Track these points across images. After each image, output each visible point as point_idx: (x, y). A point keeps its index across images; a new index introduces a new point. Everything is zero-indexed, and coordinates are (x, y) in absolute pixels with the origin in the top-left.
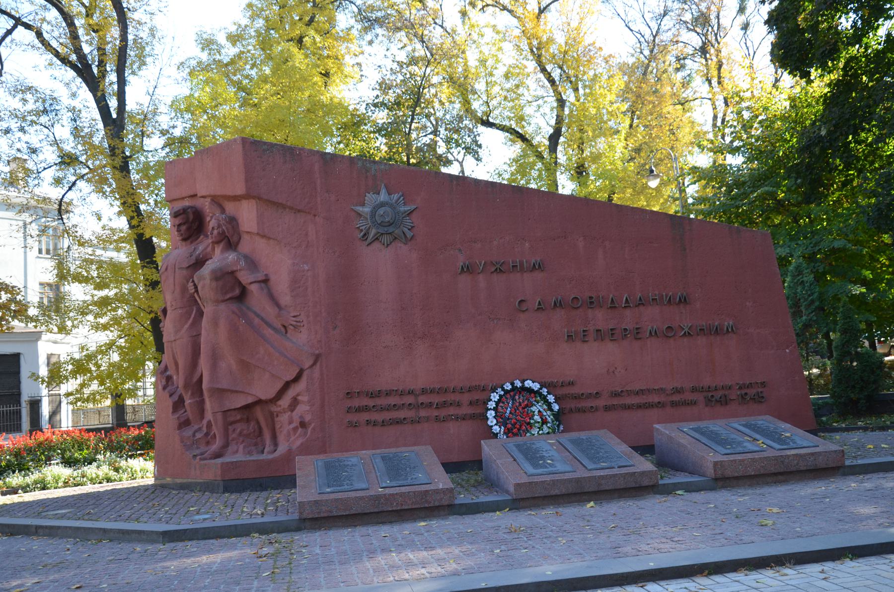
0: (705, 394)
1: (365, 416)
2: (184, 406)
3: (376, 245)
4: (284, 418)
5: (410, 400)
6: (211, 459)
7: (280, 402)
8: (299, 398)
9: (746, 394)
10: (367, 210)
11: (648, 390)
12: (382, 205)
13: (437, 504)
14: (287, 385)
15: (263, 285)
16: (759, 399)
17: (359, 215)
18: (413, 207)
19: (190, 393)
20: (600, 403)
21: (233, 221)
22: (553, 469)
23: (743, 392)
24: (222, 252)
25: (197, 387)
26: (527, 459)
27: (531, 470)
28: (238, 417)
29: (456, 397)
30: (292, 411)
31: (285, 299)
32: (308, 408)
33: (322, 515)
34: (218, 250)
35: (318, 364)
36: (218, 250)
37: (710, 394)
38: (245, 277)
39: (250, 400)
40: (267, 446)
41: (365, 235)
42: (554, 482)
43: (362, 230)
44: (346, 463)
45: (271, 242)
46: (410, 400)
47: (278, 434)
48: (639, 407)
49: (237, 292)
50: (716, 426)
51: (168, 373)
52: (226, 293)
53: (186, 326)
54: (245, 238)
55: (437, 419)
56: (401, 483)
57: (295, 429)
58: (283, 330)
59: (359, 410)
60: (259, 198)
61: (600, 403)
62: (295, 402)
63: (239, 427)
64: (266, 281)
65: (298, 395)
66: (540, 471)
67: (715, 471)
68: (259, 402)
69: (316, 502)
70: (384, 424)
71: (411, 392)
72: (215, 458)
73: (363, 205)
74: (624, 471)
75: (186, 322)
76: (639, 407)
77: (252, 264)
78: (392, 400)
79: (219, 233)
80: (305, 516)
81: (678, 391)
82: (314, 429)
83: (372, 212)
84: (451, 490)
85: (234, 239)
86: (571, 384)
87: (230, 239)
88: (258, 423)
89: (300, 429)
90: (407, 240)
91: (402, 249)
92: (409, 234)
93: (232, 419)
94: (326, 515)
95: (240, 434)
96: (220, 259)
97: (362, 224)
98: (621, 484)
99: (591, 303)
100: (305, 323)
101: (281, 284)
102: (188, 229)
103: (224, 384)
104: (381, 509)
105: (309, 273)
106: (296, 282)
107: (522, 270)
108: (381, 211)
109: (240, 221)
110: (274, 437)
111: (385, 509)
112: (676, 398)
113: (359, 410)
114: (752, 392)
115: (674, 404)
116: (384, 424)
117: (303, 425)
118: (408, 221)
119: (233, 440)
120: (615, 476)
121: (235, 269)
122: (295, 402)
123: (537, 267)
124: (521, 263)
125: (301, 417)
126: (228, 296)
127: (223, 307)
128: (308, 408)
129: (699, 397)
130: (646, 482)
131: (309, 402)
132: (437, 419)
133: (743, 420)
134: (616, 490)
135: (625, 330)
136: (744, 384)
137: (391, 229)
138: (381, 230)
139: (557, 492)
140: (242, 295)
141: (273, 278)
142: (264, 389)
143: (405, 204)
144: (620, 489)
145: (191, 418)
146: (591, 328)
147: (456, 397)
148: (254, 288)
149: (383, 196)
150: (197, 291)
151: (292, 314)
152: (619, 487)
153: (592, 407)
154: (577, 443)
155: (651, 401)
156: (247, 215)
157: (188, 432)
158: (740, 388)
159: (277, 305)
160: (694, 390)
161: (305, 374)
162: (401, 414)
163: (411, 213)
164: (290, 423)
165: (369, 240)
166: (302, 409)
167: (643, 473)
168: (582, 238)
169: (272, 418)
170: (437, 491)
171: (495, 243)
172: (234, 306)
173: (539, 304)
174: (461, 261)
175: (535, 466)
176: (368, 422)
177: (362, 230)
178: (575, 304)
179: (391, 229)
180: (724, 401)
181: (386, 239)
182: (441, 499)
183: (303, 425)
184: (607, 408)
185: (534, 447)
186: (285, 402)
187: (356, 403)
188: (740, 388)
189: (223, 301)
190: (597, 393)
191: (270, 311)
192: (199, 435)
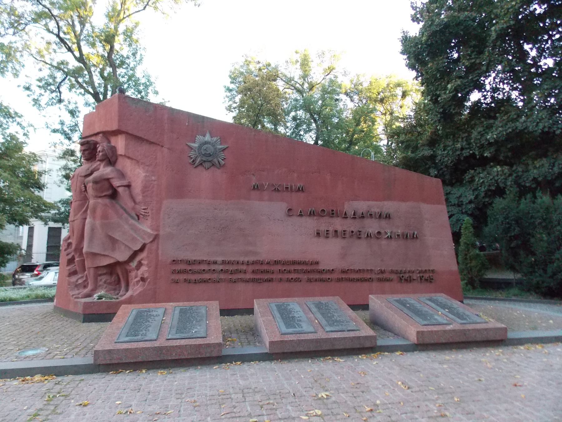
0: (399, 275)
1: (185, 276)
2: (74, 262)
3: (200, 168)
4: (133, 274)
6: (82, 298)
7: (131, 264)
8: (143, 262)
9: (423, 276)
10: (196, 145)
11: (364, 270)
12: (206, 143)
13: (208, 355)
15: (126, 188)
16: (430, 280)
17: (191, 148)
18: (226, 146)
19: (78, 254)
20: (334, 276)
21: (113, 149)
22: (300, 329)
23: (421, 275)
24: (104, 167)
25: (79, 249)
26: (283, 318)
27: (284, 329)
28: (105, 272)
29: (244, 267)
31: (139, 198)
32: (147, 269)
33: (113, 362)
34: (102, 166)
35: (156, 241)
36: (102, 166)
37: (401, 275)
38: (116, 183)
39: (112, 261)
40: (121, 291)
41: (193, 161)
42: (300, 342)
43: (192, 158)
44: (151, 313)
45: (134, 161)
47: (130, 281)
48: (358, 280)
49: (110, 192)
50: (411, 299)
51: (69, 241)
52: (102, 192)
53: (80, 213)
54: (120, 160)
55: (231, 281)
56: (183, 335)
57: (138, 282)
58: (136, 218)
59: (180, 272)
60: (126, 133)
61: (334, 276)
63: (104, 278)
64: (129, 186)
65: (142, 260)
66: (290, 330)
67: (418, 338)
69: (109, 351)
70: (195, 282)
72: (85, 297)
73: (194, 142)
74: (352, 334)
75: (81, 211)
76: (358, 280)
77: (122, 175)
78: (203, 267)
79: (102, 155)
80: (99, 362)
81: (382, 272)
82: (149, 283)
83: (199, 146)
84: (219, 345)
85: (113, 160)
87: (111, 159)
88: (118, 275)
89: (141, 282)
90: (221, 166)
91: (218, 172)
92: (223, 162)
93: (100, 272)
94: (116, 362)
95: (105, 282)
96: (105, 171)
97: (192, 154)
98: (349, 345)
99: (333, 214)
100: (150, 214)
101: (137, 188)
102: (89, 153)
103: (96, 250)
104: (162, 358)
105: (155, 183)
106: (145, 189)
107: (292, 191)
108: (205, 147)
109: (117, 148)
110: (127, 285)
111: (166, 358)
112: (380, 276)
113: (180, 272)
114: (426, 276)
115: (380, 280)
116: (195, 282)
117: (143, 279)
118: (222, 155)
119: (100, 286)
120: (345, 338)
121: (110, 177)
122: (140, 264)
123: (300, 190)
124: (291, 187)
125: (143, 274)
126: (104, 194)
127: (100, 200)
128: (147, 269)
129: (393, 276)
130: (368, 345)
131: (148, 264)
132: (231, 281)
133: (428, 296)
134: (345, 349)
135: (352, 232)
136: (422, 270)
137: (210, 159)
138: (204, 159)
139: (302, 349)
140: (114, 195)
141: (133, 184)
142: (121, 256)
143: (221, 144)
144: (348, 349)
145: (78, 270)
146: (331, 229)
147: (244, 267)
148: (120, 190)
149: (208, 138)
151: (143, 208)
152: (348, 347)
153: (329, 279)
154: (319, 306)
155: (365, 276)
156: (120, 143)
157: (74, 279)
158: (419, 273)
159: (134, 202)
160: (392, 272)
161: (147, 246)
162: (206, 276)
164: (136, 277)
165: (196, 164)
166: (144, 268)
167: (366, 338)
168: (329, 174)
169: (127, 273)
170: (209, 345)
171: (276, 172)
172: (107, 201)
173: (301, 212)
174: (254, 181)
175: (288, 325)
176: (185, 280)
177: (192, 158)
178: (321, 214)
179: (210, 159)
180: (409, 280)
181: (207, 165)
182: (212, 351)
183: (143, 279)
184: (339, 280)
185: (289, 307)
186: (134, 264)
188: (419, 273)
189: (100, 197)
190: (333, 270)
191: (130, 204)
192: (80, 281)
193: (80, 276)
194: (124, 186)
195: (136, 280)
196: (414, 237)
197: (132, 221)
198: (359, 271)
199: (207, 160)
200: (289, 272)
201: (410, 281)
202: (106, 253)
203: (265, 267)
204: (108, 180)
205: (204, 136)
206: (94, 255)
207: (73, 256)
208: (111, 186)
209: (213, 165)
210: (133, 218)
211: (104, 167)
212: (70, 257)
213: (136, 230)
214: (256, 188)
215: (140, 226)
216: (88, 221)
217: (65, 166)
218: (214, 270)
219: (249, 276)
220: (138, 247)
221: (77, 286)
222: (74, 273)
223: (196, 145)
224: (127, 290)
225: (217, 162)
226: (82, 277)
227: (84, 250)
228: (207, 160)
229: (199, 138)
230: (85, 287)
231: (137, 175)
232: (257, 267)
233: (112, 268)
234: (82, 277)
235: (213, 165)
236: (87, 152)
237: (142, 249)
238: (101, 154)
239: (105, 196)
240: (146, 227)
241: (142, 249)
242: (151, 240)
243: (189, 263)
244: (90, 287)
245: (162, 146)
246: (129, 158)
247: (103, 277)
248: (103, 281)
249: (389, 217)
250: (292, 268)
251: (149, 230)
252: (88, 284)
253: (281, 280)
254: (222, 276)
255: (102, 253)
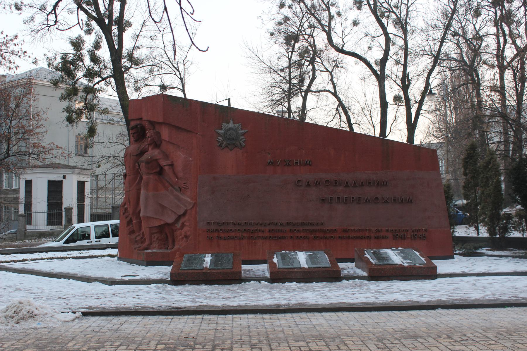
5: (237, 228)
7: (176, 225)
8: (185, 223)
12: (230, 129)
14: (180, 217)
17: (219, 134)
24: (152, 149)
29: (262, 228)
30: (182, 229)
31: (181, 175)
32: (189, 229)
34: (150, 148)
38: (163, 163)
39: (162, 223)
41: (221, 144)
46: (237, 228)
48: (357, 238)
49: (158, 169)
51: (126, 207)
57: (182, 238)
62: (183, 225)
64: (172, 165)
65: (185, 222)
68: (167, 224)
71: (239, 224)
73: (221, 129)
77: (166, 156)
78: (231, 227)
86: (322, 224)
88: (166, 234)
89: (185, 239)
92: (244, 144)
93: (154, 231)
95: (157, 239)
96: (152, 153)
97: (220, 139)
101: (179, 166)
103: (149, 215)
108: (229, 133)
110: (174, 241)
113: (213, 231)
119: (154, 241)
121: (157, 158)
122: (183, 225)
124: (300, 162)
126: (154, 171)
127: (151, 176)
128: (189, 229)
140: (161, 172)
141: (175, 164)
142: (170, 220)
143: (242, 129)
148: (166, 168)
149: (231, 125)
150: (139, 168)
156: (165, 133)
157: (133, 236)
160: (388, 231)
163: (244, 134)
166: (186, 229)
180: (403, 238)
183: (186, 237)
186: (179, 225)
187: (213, 227)
189: (151, 174)
192: (138, 238)
193: (137, 234)
194: (169, 165)
195: (181, 237)
196: (410, 201)
197: (176, 193)
198: (358, 231)
199: (231, 142)
200: (299, 231)
201: (405, 239)
202: (158, 217)
203: (280, 228)
204: (156, 160)
205: (228, 123)
206: (148, 218)
207: (131, 219)
208: (159, 165)
209: (236, 146)
210: (176, 190)
211: (152, 149)
212: (128, 219)
213: (179, 199)
214: (273, 164)
215: (182, 197)
216: (142, 192)
217: (67, 108)
218: (239, 230)
219: (267, 234)
220: (181, 212)
221: (136, 242)
222: (133, 232)
223: (221, 131)
224: (174, 245)
225: (239, 144)
226: (139, 235)
227: (141, 215)
228: (231, 142)
229: (225, 125)
230: (142, 242)
231: (180, 157)
232: (272, 227)
233: (162, 228)
234: (139, 235)
235: (236, 146)
236: (135, 135)
237: (184, 214)
238: (149, 139)
239: (154, 173)
240: (187, 198)
241: (184, 214)
242: (191, 207)
243: (219, 224)
244: (147, 243)
245: (197, 134)
246: (171, 143)
247: (155, 235)
248: (156, 238)
249: (323, 200)
250: (301, 228)
251: (189, 200)
252: (145, 239)
253: (292, 238)
254: (245, 235)
255: (155, 217)
